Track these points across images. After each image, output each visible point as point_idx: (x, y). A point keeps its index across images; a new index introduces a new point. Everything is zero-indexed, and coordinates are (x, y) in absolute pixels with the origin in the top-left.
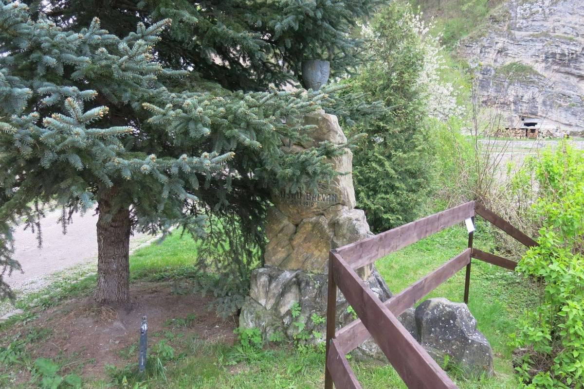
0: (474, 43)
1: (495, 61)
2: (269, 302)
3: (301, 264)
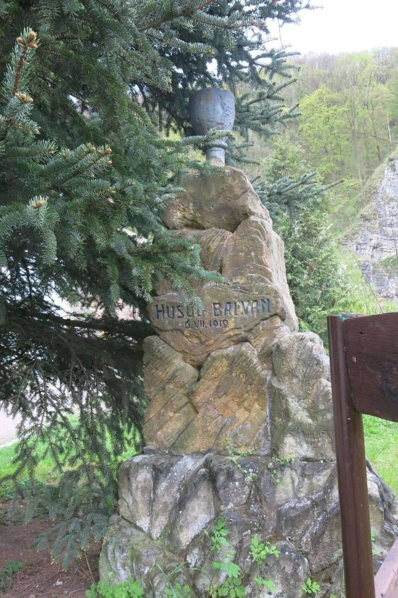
0: (350, 241)
1: (372, 256)
2: (157, 523)
3: (212, 440)
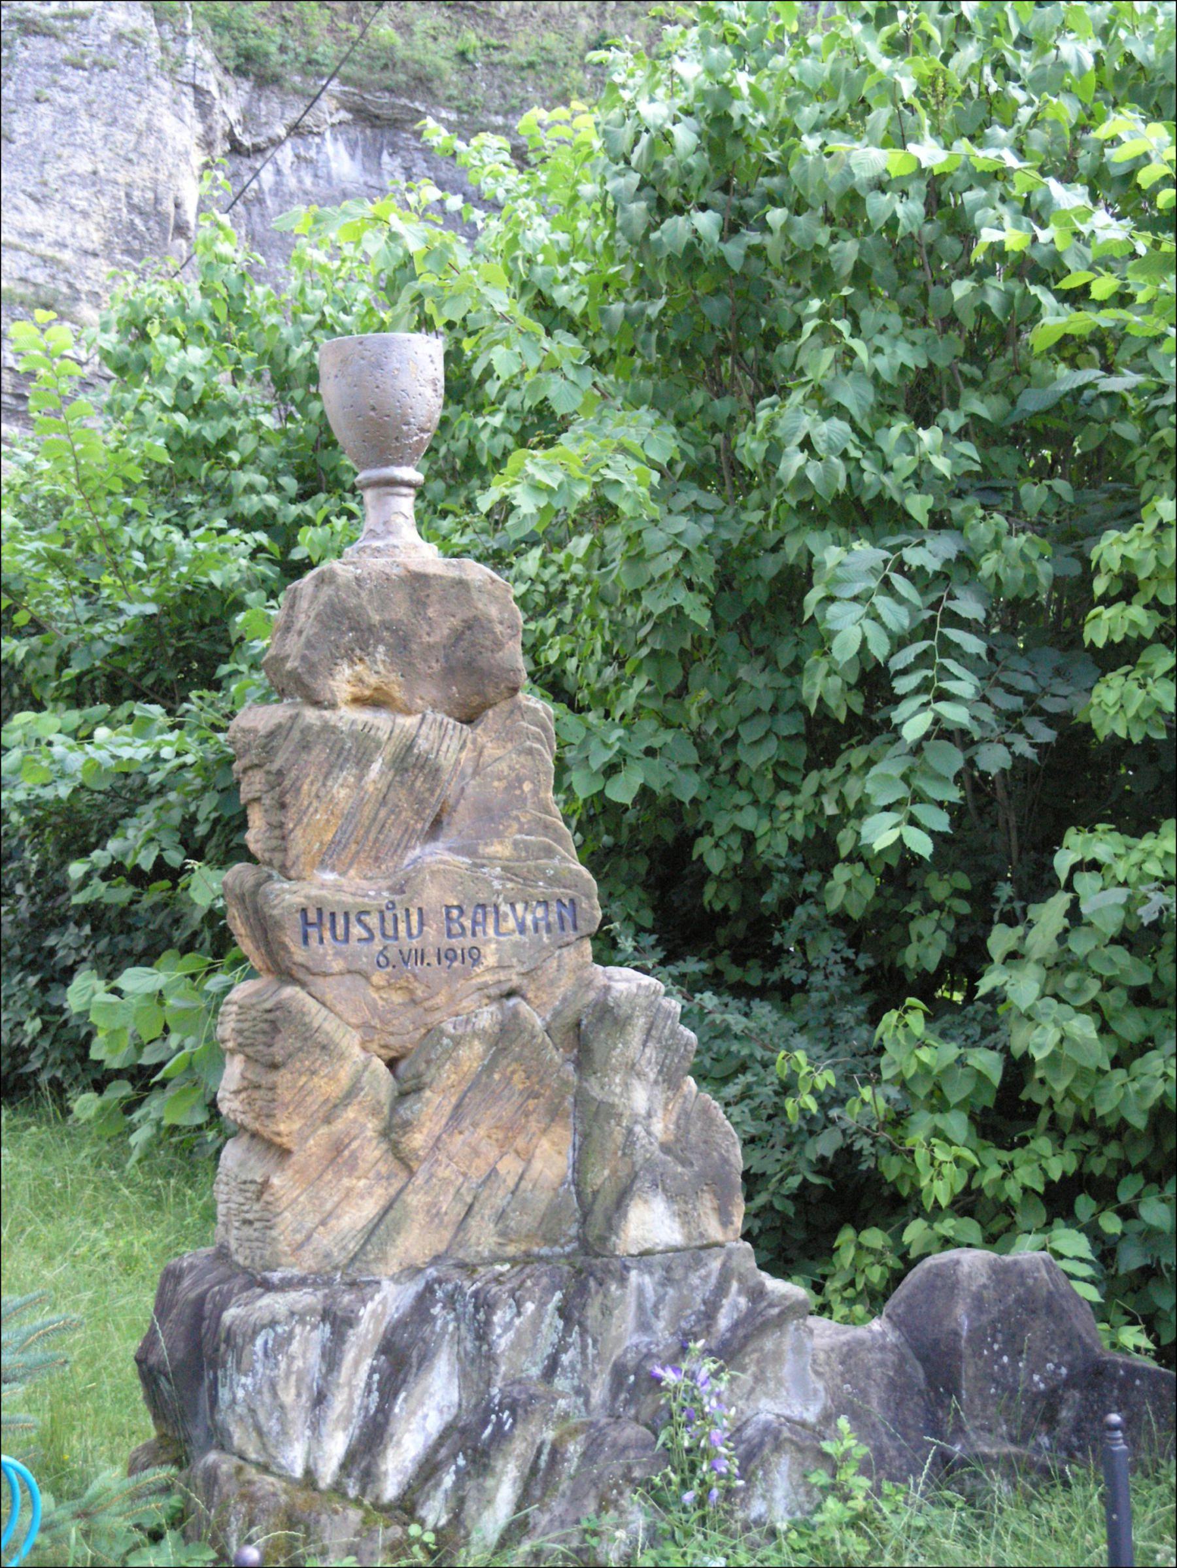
3: (448, 1234)
